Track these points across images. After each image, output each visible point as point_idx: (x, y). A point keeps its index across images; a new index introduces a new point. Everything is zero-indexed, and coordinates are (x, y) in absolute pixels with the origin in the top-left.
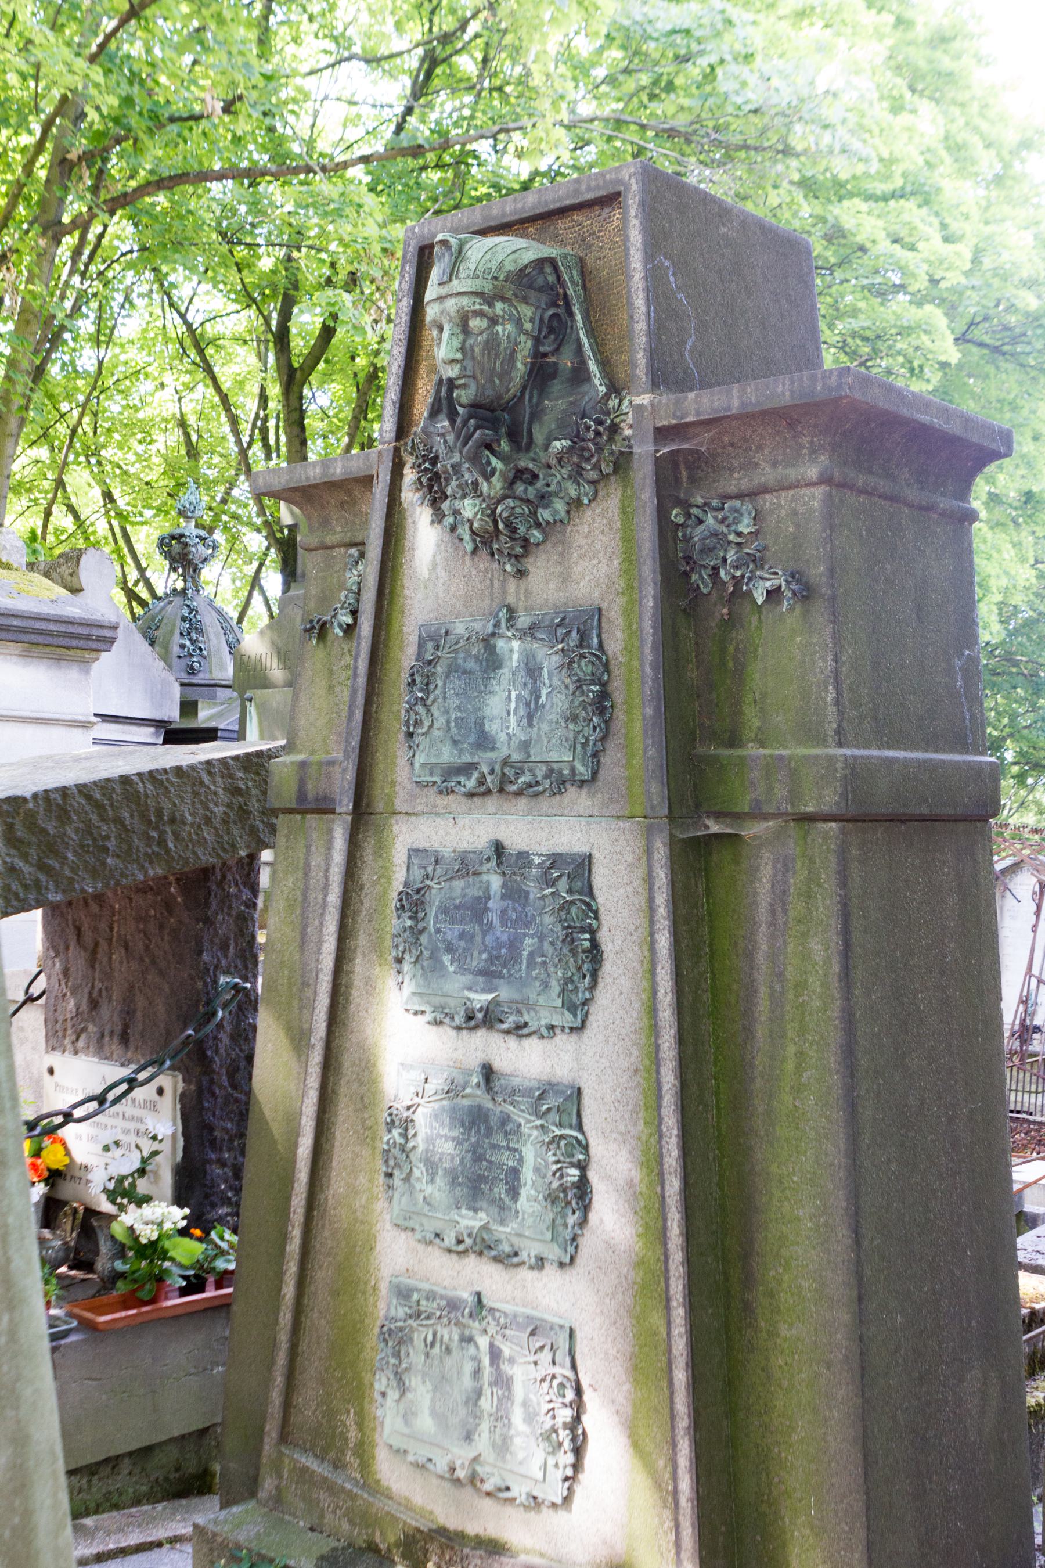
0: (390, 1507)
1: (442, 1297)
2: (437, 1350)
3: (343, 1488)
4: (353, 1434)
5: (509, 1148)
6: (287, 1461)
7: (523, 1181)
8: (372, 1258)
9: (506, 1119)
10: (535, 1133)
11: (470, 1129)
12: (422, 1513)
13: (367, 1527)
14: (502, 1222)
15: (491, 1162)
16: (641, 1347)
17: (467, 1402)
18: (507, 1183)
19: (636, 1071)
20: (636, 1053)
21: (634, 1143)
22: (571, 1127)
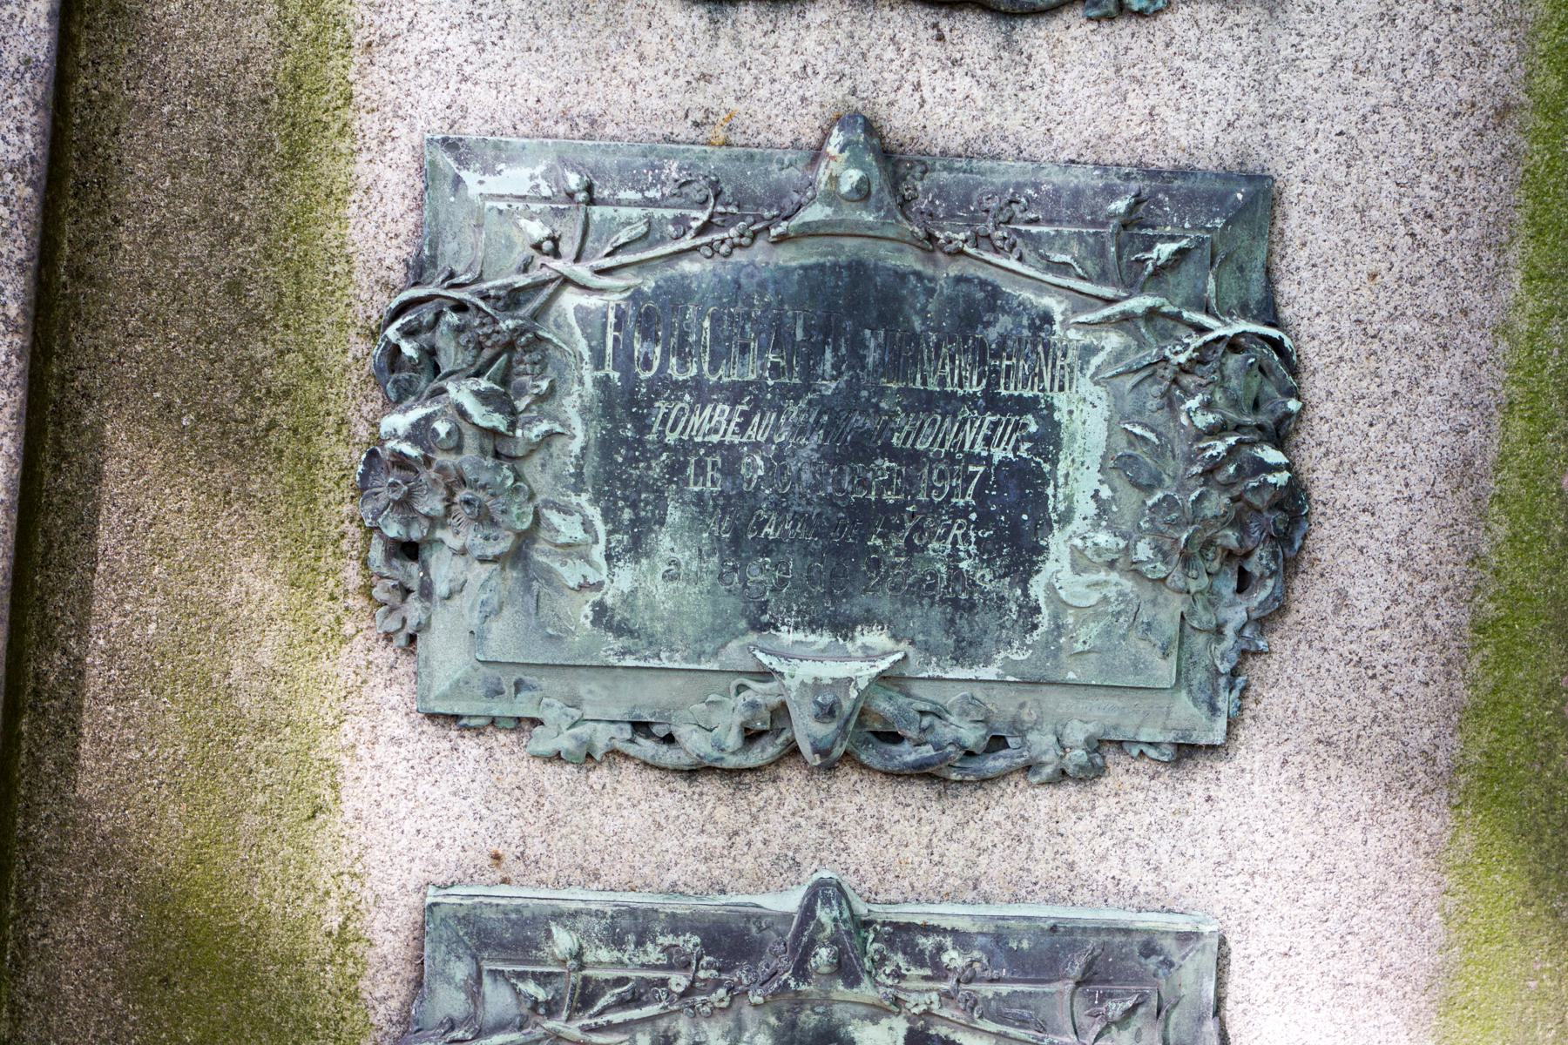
1: (676, 925)
5: (992, 402)
7: (1055, 501)
8: (322, 846)
9: (976, 307)
10: (1113, 340)
11: (816, 352)
14: (964, 652)
15: (914, 457)
18: (984, 520)
19: (1503, 112)
20: (1504, 52)
21: (1480, 342)
22: (1244, 311)
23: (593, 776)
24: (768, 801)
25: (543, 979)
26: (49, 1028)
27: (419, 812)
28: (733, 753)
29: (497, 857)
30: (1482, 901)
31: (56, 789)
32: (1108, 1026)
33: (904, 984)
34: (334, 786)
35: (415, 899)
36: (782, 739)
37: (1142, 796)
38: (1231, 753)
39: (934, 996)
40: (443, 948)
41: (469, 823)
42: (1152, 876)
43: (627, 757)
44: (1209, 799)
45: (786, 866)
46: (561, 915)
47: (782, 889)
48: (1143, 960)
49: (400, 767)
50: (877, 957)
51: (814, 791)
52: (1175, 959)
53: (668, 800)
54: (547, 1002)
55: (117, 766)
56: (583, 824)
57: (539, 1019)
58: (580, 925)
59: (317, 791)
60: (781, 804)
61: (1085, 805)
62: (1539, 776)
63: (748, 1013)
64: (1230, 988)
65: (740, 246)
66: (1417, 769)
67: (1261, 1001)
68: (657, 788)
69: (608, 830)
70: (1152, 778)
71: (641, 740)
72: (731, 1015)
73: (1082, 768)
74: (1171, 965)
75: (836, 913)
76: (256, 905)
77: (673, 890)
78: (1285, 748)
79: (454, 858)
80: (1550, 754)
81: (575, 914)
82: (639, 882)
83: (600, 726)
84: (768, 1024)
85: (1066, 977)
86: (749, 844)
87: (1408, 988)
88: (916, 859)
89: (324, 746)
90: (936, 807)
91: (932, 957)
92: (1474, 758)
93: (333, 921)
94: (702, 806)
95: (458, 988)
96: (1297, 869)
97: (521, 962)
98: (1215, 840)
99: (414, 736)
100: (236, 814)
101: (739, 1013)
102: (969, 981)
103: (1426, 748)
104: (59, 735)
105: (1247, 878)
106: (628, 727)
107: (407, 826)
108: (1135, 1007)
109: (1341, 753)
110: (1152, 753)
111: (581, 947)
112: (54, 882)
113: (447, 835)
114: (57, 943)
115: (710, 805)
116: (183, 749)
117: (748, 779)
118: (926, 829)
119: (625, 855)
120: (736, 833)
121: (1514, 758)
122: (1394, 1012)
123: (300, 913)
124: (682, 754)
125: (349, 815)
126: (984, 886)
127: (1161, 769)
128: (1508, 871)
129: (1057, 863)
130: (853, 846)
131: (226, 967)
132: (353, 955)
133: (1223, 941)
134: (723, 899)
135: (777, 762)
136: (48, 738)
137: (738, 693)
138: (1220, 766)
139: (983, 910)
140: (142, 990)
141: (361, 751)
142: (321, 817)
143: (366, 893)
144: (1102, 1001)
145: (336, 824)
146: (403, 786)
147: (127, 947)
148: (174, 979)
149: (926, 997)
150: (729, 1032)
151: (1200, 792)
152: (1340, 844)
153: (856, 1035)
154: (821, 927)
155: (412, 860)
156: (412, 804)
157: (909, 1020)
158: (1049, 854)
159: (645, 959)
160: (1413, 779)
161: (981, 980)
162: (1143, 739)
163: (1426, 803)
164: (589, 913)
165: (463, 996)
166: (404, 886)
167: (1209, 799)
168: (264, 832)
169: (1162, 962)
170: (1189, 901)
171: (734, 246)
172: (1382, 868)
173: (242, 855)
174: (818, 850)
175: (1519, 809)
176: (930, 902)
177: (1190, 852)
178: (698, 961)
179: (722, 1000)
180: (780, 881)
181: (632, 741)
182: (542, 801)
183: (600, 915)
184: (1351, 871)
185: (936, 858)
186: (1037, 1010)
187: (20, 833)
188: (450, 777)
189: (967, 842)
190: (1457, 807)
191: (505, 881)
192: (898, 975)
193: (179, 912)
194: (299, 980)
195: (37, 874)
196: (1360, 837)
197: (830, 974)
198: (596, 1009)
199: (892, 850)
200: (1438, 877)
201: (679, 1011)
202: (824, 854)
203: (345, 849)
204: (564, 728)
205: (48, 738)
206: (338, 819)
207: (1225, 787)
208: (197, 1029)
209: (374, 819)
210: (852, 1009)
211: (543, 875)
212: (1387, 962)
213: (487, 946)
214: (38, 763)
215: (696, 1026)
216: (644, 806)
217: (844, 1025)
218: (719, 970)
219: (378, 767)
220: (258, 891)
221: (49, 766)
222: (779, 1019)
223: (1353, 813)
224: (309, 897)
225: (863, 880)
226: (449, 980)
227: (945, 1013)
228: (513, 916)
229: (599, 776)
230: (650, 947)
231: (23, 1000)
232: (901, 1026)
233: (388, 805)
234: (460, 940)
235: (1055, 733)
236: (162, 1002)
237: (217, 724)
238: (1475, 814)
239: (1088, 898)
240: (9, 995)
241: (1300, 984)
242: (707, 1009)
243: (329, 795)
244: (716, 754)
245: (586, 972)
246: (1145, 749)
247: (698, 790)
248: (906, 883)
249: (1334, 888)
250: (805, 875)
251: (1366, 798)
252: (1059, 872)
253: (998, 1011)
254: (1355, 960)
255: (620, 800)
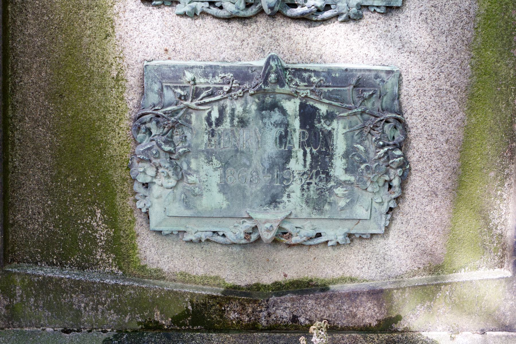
0: (169, 286)
1: (225, 70)
2: (227, 124)
3: (105, 286)
4: (102, 232)
6: (18, 280)
8: (109, 48)
12: (205, 280)
13: (142, 310)
16: (479, 76)
17: (270, 170)
23: (197, 21)
24: (254, 29)
25: (183, 88)
26: (25, 112)
27: (140, 35)
28: (242, 10)
29: (166, 50)
30: (483, 61)
31: (21, 30)
32: (363, 101)
33: (298, 88)
34: (113, 27)
35: (140, 65)
36: (258, 6)
37: (375, 26)
38: (404, 11)
39: (308, 91)
40: (150, 80)
41: (157, 39)
42: (378, 53)
43: (208, 14)
44: (396, 27)
45: (260, 51)
46: (188, 68)
47: (258, 59)
48: (375, 80)
49: (134, 20)
50: (290, 79)
51: (269, 25)
52: (385, 80)
53: (221, 29)
54: (184, 96)
55: (41, 22)
56: (194, 38)
57: (182, 101)
58: (194, 71)
59: (107, 29)
60: (258, 30)
61: (356, 29)
62: (503, 17)
63: (249, 98)
64: (403, 91)
65: (240, 97)
66: (464, 15)
67: (412, 95)
68: (218, 25)
69: (202, 40)
70: (378, 19)
71: (212, 8)
72: (243, 99)
73: (355, 15)
74: (384, 81)
75: (276, 63)
76: (89, 69)
77: (224, 61)
78: (421, 9)
79: (153, 51)
80: (507, 10)
81: (192, 68)
82: (212, 58)
83: (199, 3)
84: (255, 101)
85: (350, 85)
86: (248, 44)
87: (459, 90)
88: (302, 48)
89: (108, 13)
90: (308, 30)
91: (307, 79)
92: (483, 11)
93: (114, 74)
94: (232, 31)
95: (156, 93)
96: (424, 50)
97: (175, 83)
98: (398, 41)
99: (138, 9)
100: (81, 38)
101: (246, 98)
102: (319, 87)
103: (467, 8)
104: (21, 12)
105: (408, 54)
106: (208, 3)
107: (137, 40)
108: (373, 94)
109: (439, 10)
110: (378, 10)
111: (195, 78)
112: (23, 63)
113: (150, 43)
114: (25, 83)
115: (235, 31)
116: (62, 16)
117: (247, 21)
118: (305, 38)
119: (208, 49)
120: (244, 41)
121: (495, 11)
122: (455, 98)
123: (103, 71)
124: (225, 12)
125: (118, 37)
126: (324, 57)
127: (381, 16)
128: (492, 51)
129: (347, 49)
130: (281, 44)
131: (80, 90)
132: (121, 85)
133: (400, 75)
134: (240, 63)
135: (256, 15)
136: (17, 13)
137: (243, 223)
138: (400, 15)
139: (323, 65)
140: (54, 99)
141: (121, 15)
142: (109, 38)
143: (125, 64)
144: (362, 93)
145: (114, 40)
146: (135, 27)
147: (48, 84)
148: (64, 95)
149: (306, 91)
150: (243, 105)
151: (393, 24)
152: (438, 41)
153: (284, 105)
154: (272, 67)
155: (139, 52)
156: (138, 33)
157: (300, 99)
158: (345, 46)
159: (215, 81)
160: (462, 19)
161: (323, 86)
162: (375, 5)
163: (466, 27)
164: (197, 67)
165: (157, 96)
166: (137, 61)
167: (396, 27)
168: (90, 44)
169: (381, 81)
170: (390, 62)
171: (238, 96)
172: (452, 50)
173: (84, 52)
174: (270, 46)
175: (496, 29)
176: (306, 63)
177: (390, 45)
178: (233, 81)
179: (240, 93)
180: (258, 56)
181: (209, 8)
182: (180, 30)
183: (201, 67)
184: (442, 51)
185: (308, 48)
186: (341, 96)
187: (10, 46)
188: (150, 23)
189: (318, 42)
190: (477, 28)
191: (169, 59)
192: (296, 85)
193: (64, 72)
194: (104, 94)
195: (17, 60)
196: (445, 39)
197: (275, 83)
198: (200, 98)
199: (294, 45)
200: (470, 53)
201: (227, 98)
202: (272, 47)
203: (117, 49)
204: (187, 3)
205: (17, 13)
206: (114, 39)
207: (402, 22)
208: (72, 111)
209: (126, 38)
210: (282, 96)
211: (182, 56)
212: (453, 82)
213: (164, 78)
214: (15, 22)
215: (232, 103)
216: (214, 31)
217: (280, 101)
218: (239, 84)
219: (126, 20)
220: (89, 64)
221: (19, 23)
222: (259, 100)
223: (443, 31)
224: (106, 66)
225: (285, 56)
226: (152, 91)
227: (312, 97)
228: (172, 69)
229: (199, 22)
230: (217, 77)
231: (16, 103)
232: (298, 101)
233: (130, 33)
234: (155, 77)
235: (347, 3)
236: (60, 103)
237: (73, 6)
238: (482, 31)
239: (357, 61)
240: (11, 102)
241: (425, 89)
242: (236, 97)
243: (111, 30)
244: (237, 11)
245: (197, 86)
246: (376, 8)
247: (231, 26)
248: (299, 57)
249: (436, 57)
250: (266, 54)
251: (447, 26)
252: (348, 52)
253: (329, 96)
254: (443, 81)
255: (206, 30)
